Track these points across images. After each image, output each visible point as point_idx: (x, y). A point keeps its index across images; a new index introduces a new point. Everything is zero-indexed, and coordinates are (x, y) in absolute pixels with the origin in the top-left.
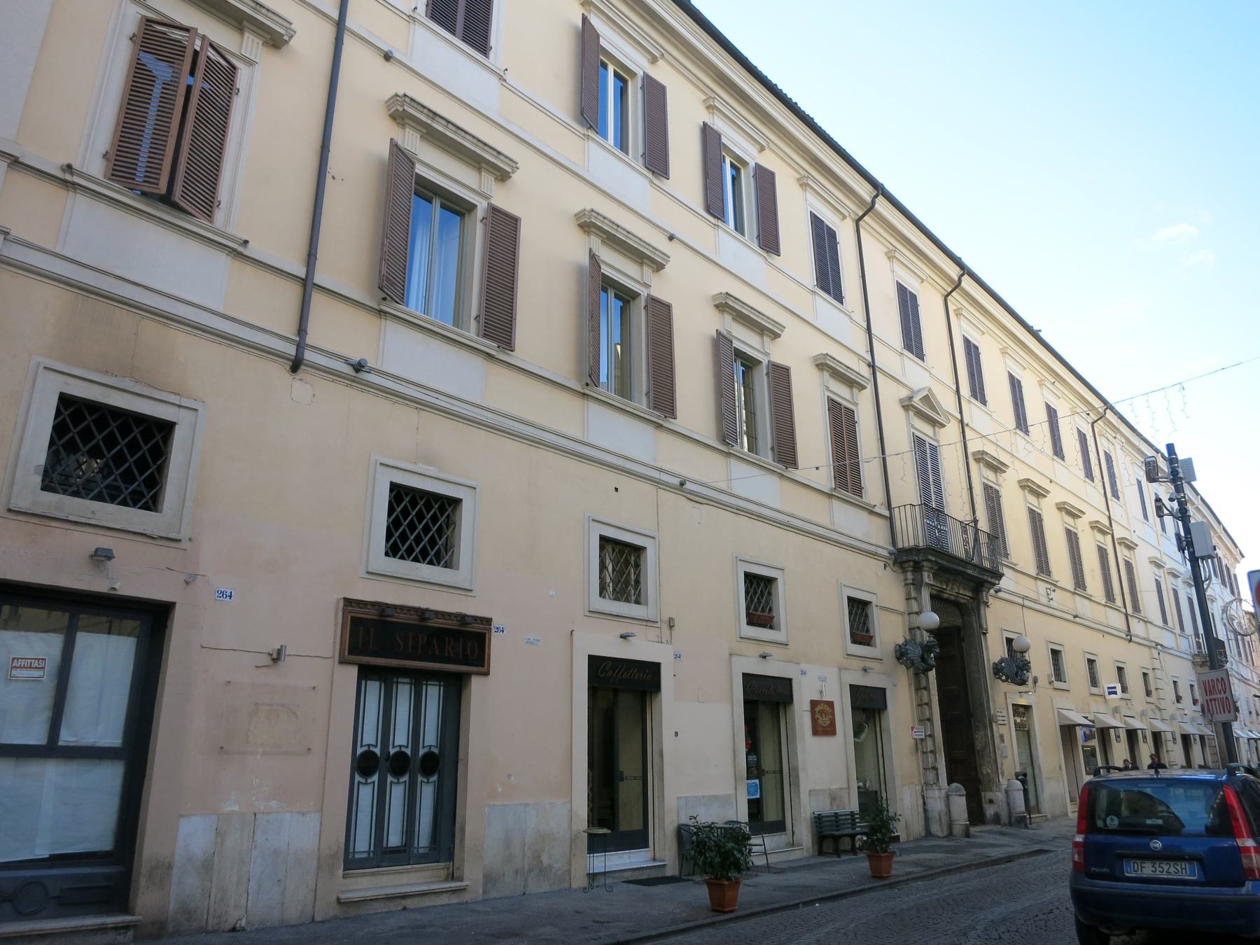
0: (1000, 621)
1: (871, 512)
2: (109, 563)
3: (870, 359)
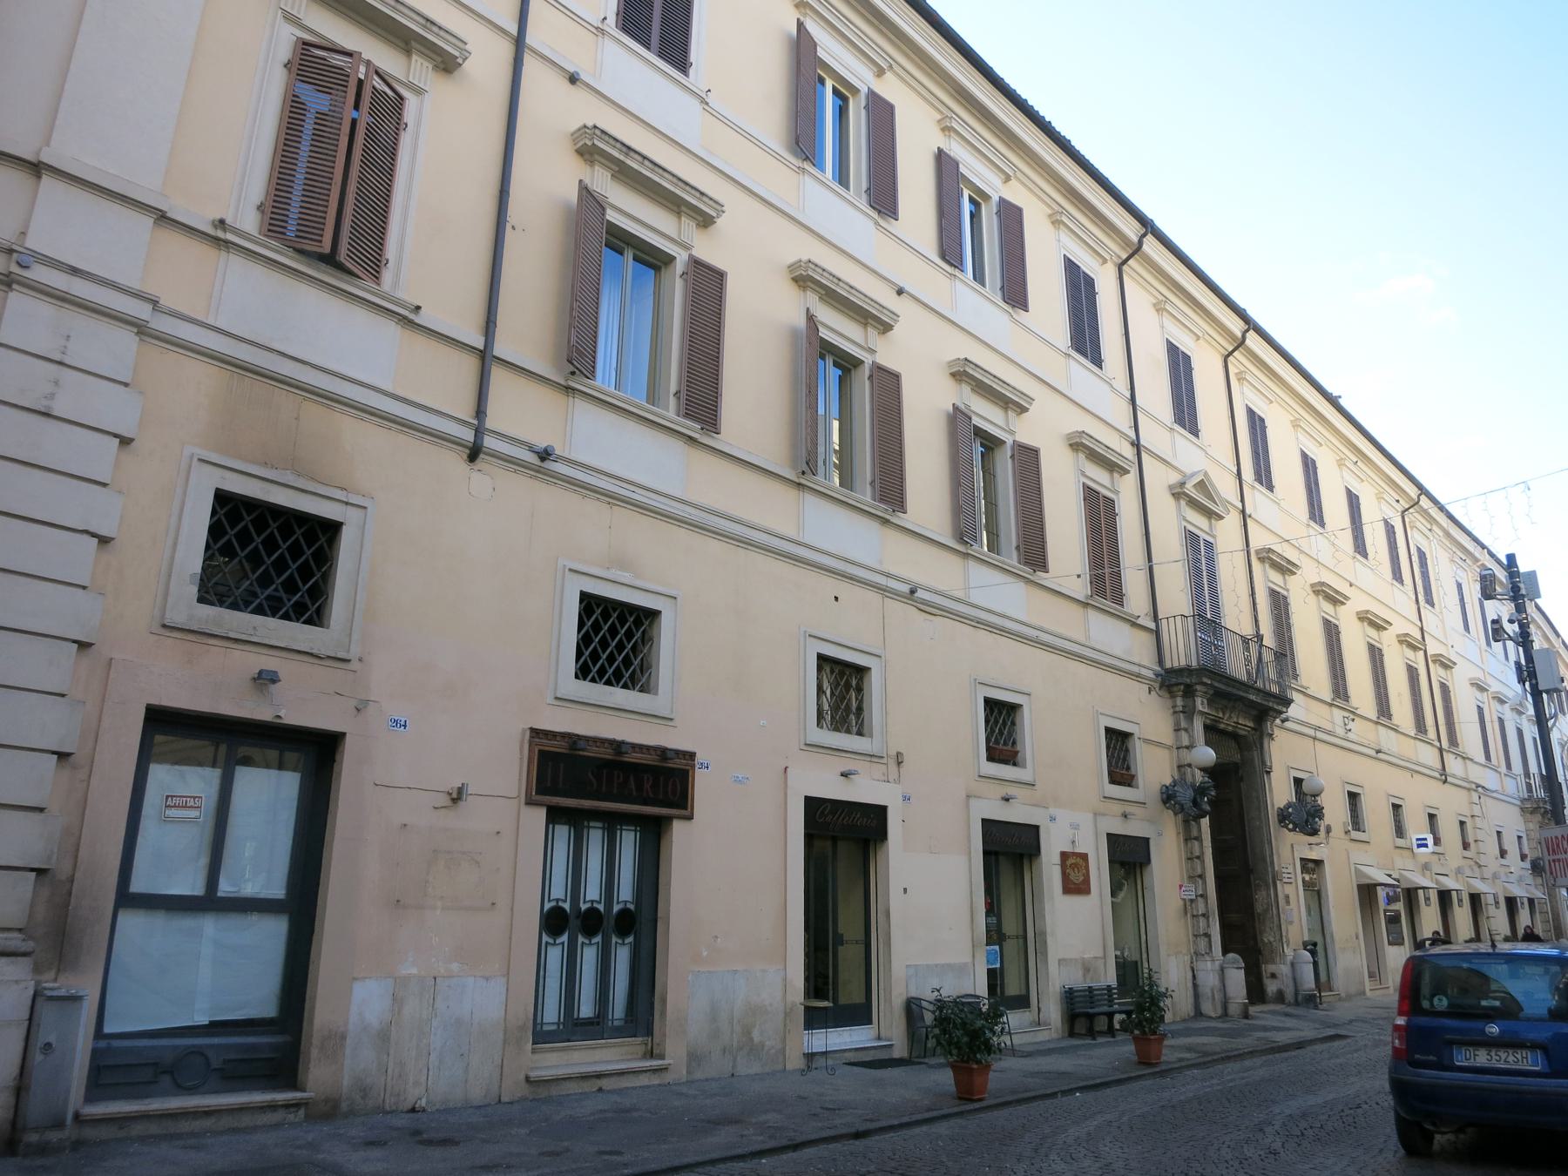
0: (1287, 756)
1: (1134, 624)
2: (273, 688)
3: (1132, 435)
